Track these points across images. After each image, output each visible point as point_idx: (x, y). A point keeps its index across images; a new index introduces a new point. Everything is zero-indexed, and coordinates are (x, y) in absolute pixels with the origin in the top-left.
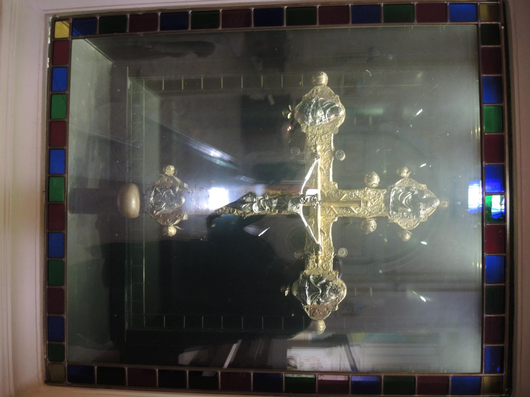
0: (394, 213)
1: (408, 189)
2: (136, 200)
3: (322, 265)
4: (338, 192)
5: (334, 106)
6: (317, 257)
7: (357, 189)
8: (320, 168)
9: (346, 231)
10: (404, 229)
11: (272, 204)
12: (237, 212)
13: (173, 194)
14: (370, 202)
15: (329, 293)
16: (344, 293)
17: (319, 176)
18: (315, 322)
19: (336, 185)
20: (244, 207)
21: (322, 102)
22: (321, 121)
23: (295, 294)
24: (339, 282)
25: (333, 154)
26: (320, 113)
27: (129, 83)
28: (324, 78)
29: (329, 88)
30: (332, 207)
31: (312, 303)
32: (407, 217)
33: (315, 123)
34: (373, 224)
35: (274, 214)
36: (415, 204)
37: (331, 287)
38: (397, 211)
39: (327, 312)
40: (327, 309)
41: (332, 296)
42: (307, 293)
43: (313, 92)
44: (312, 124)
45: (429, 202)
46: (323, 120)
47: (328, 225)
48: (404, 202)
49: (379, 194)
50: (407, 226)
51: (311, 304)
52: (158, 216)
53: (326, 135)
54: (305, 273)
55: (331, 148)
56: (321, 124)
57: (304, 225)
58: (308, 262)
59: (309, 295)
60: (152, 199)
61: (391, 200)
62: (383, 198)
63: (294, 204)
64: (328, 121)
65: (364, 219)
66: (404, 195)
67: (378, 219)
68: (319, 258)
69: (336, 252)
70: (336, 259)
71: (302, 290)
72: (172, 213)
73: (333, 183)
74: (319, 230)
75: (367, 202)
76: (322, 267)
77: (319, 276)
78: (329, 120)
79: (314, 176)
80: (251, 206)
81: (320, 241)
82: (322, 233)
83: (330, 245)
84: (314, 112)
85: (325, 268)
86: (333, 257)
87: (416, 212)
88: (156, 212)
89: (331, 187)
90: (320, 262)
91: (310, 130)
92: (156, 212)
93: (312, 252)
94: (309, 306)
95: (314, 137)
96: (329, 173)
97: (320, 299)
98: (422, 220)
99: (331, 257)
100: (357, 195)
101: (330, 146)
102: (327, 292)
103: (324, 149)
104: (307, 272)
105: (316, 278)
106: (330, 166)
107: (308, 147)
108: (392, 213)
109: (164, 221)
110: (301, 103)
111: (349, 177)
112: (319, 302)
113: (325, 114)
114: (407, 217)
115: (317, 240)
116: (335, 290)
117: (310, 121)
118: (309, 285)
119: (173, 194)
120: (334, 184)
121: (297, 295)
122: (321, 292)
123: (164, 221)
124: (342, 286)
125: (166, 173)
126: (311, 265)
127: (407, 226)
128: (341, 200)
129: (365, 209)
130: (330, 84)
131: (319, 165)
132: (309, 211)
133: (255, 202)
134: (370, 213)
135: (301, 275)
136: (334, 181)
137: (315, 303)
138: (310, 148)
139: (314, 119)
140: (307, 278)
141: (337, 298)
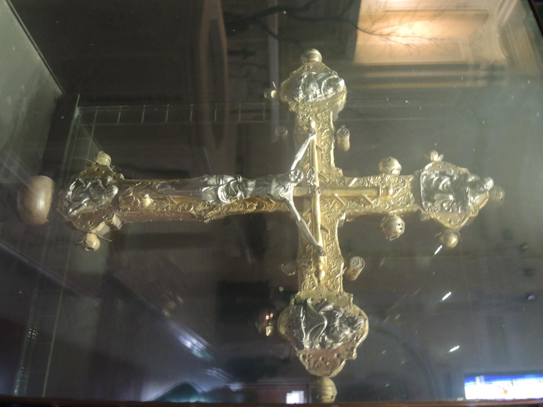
0: (429, 204)
1: (443, 174)
2: (46, 201)
3: (326, 283)
4: (344, 179)
5: (331, 77)
6: (318, 267)
7: (370, 175)
8: (317, 147)
9: (360, 234)
10: (446, 228)
11: (247, 186)
12: (194, 209)
13: (101, 185)
14: (391, 193)
15: (341, 326)
16: (364, 325)
17: (317, 147)
18: (318, 381)
19: (341, 171)
20: (205, 191)
21: (316, 76)
22: (315, 96)
23: (282, 330)
24: (354, 310)
25: (334, 135)
26: (314, 88)
27: (77, 112)
28: (317, 56)
29: (323, 64)
30: (336, 195)
31: (311, 346)
32: (449, 210)
33: (308, 98)
34: (399, 226)
35: (250, 210)
36: (459, 190)
37: (344, 315)
38: (433, 202)
39: (339, 361)
40: (338, 356)
41: (346, 329)
42: (303, 328)
43: (303, 68)
44: (303, 101)
45: (476, 187)
46: (318, 96)
47: (333, 223)
48: (440, 187)
49: (404, 182)
50: (450, 222)
51: (311, 347)
52: (75, 218)
53: (323, 113)
54: (299, 297)
55: (330, 127)
56: (315, 101)
57: (297, 219)
58: (303, 280)
59: (307, 330)
60: (70, 193)
61: (422, 188)
62: (409, 187)
63: (280, 184)
64: (324, 98)
65: (385, 215)
66: (440, 180)
67: (406, 217)
68: (321, 267)
69: (347, 265)
70: (346, 279)
71: (294, 324)
72: (96, 213)
73: (335, 169)
74: (319, 227)
75: (387, 188)
76: (327, 286)
77: (322, 300)
78: (326, 96)
79: (309, 159)
80: (216, 190)
81: (321, 243)
82: (324, 224)
83: (337, 252)
84: (306, 86)
85: (331, 288)
86: (342, 272)
87: (461, 199)
88: (73, 211)
89: (334, 173)
90: (323, 274)
91: (301, 108)
92: (73, 211)
93: (310, 263)
94: (306, 351)
95: (307, 116)
96: (330, 156)
97: (326, 338)
98: (471, 215)
99: (339, 271)
100: (372, 183)
101: (329, 125)
102: (337, 323)
103: (321, 129)
104: (301, 294)
105: (317, 304)
106: (330, 149)
107: (299, 126)
108: (426, 204)
109: (81, 224)
110: (288, 79)
111: (357, 162)
112: (323, 344)
113: (320, 88)
114: (449, 210)
115: (317, 239)
116: (351, 322)
117: (301, 96)
118: (305, 314)
119: (101, 185)
120: (338, 171)
121: (286, 333)
122: (326, 323)
123: (81, 224)
124: (360, 315)
125: (97, 161)
126: (308, 283)
127: (450, 222)
128: (350, 185)
129: (385, 201)
130: (325, 59)
131: (316, 143)
132: (304, 201)
133: (222, 185)
134: (393, 206)
135: (293, 301)
136: (336, 166)
137: (318, 346)
138: (302, 127)
139: (306, 94)
140: (304, 303)
141: (353, 336)
